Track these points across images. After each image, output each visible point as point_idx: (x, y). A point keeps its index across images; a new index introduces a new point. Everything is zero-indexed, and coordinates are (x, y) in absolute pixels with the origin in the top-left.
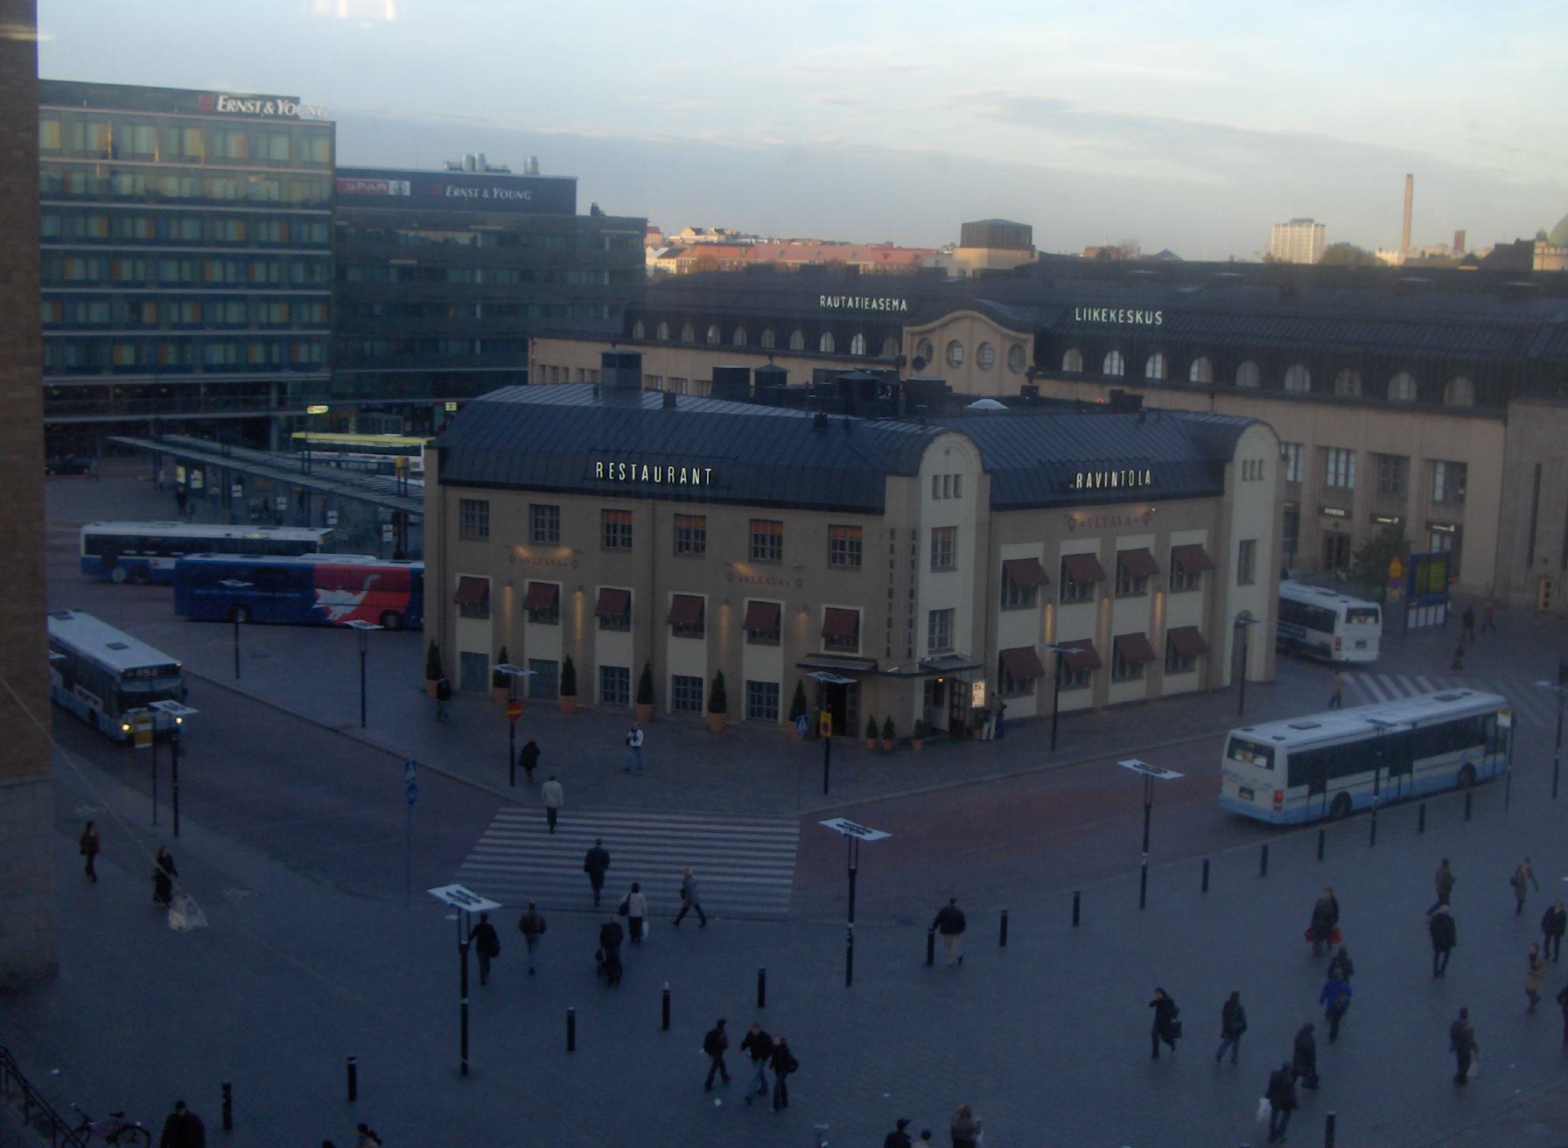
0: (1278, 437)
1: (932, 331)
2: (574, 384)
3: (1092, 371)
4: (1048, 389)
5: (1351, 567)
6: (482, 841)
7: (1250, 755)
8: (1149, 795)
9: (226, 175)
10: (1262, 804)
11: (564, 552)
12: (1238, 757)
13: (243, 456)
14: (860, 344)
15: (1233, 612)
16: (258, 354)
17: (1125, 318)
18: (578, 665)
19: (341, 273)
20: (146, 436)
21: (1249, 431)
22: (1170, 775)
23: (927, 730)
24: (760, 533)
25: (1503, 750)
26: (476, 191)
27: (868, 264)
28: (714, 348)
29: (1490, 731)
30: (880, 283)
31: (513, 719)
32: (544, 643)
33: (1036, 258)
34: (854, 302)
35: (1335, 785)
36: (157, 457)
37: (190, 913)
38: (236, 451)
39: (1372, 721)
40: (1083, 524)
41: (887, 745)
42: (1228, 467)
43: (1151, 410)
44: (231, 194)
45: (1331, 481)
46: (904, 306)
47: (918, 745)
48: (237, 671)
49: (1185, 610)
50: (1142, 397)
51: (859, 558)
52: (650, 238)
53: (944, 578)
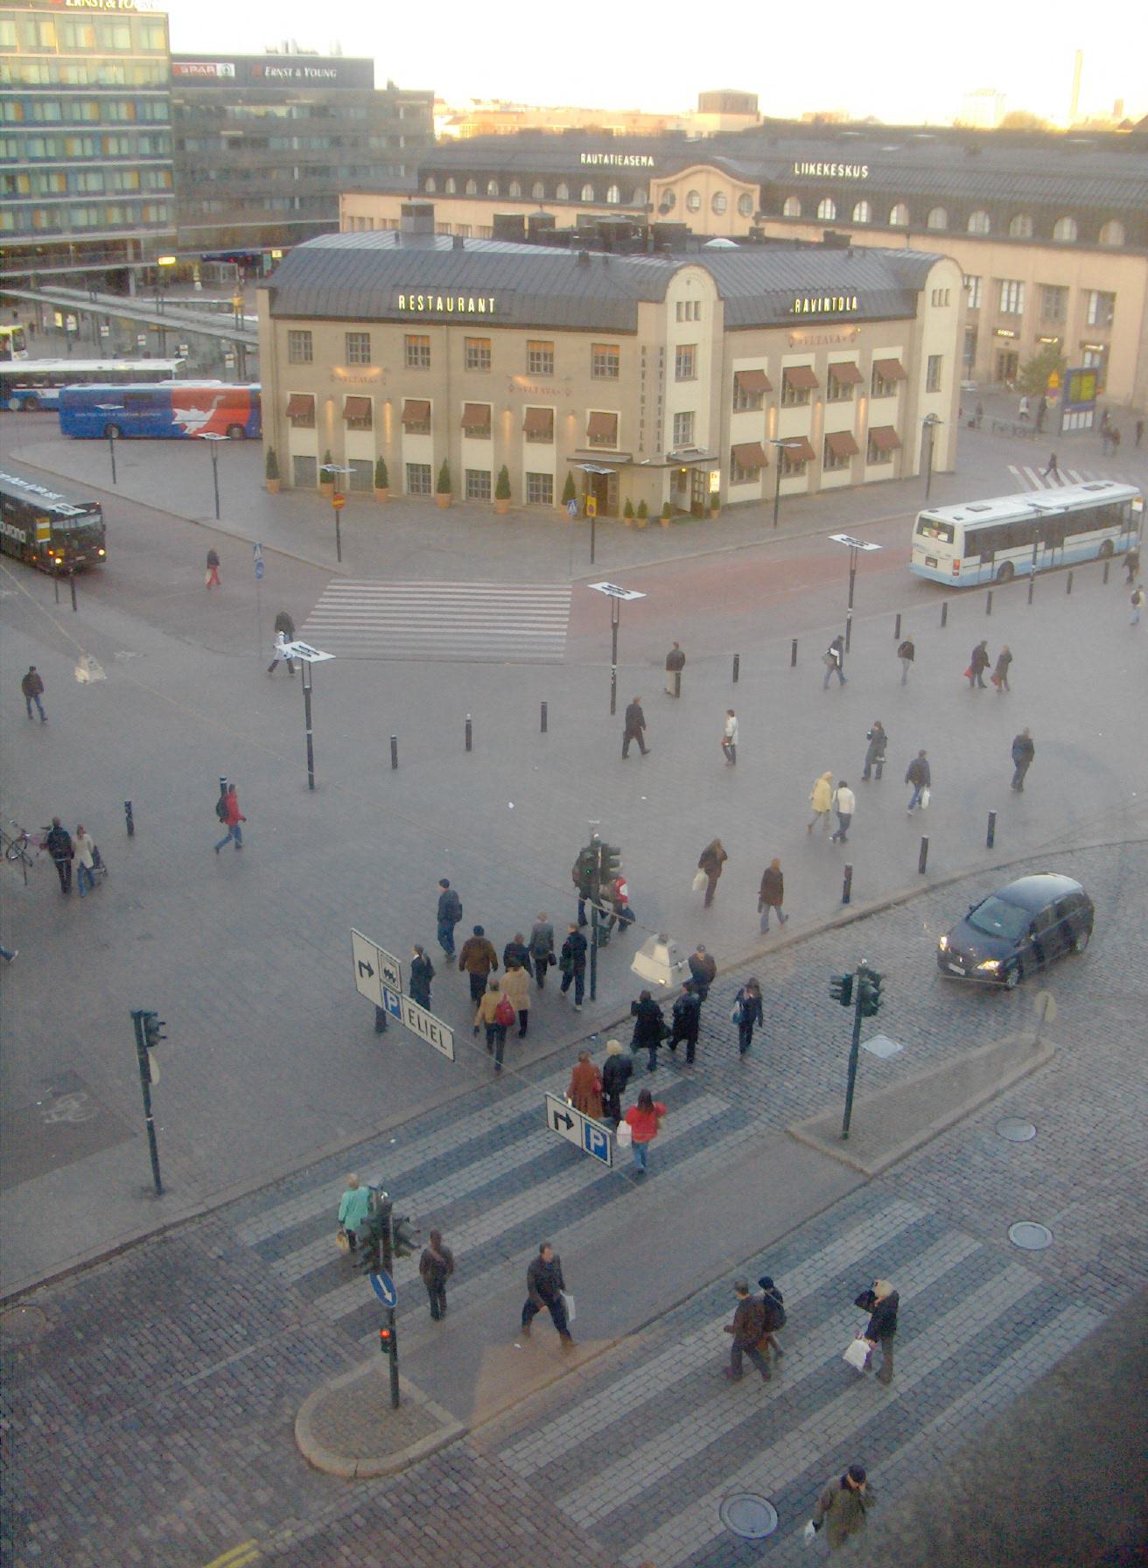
0: (961, 270)
1: (675, 183)
2: (378, 231)
3: (809, 215)
4: (773, 230)
5: (1018, 378)
6: (321, 600)
7: (935, 532)
8: (853, 566)
9: (80, 63)
10: (944, 572)
11: (374, 371)
12: (925, 533)
13: (107, 302)
14: (615, 195)
15: (923, 414)
16: (115, 216)
17: (837, 172)
18: (387, 463)
19: (181, 144)
20: (28, 289)
21: (939, 266)
22: (871, 547)
23: (672, 511)
24: (536, 351)
25: (1136, 530)
26: (290, 70)
27: (619, 128)
28: (492, 199)
29: (1126, 515)
30: (631, 144)
31: (338, 507)
32: (360, 446)
33: (761, 122)
34: (609, 159)
35: (1001, 556)
36: (38, 304)
37: (91, 669)
38: (101, 297)
39: (1034, 505)
40: (801, 341)
41: (641, 523)
42: (920, 295)
43: (858, 247)
44: (84, 81)
45: (1004, 308)
46: (651, 162)
47: (665, 522)
48: (115, 479)
49: (883, 412)
50: (850, 236)
51: (616, 370)
52: (437, 108)
53: (686, 386)
